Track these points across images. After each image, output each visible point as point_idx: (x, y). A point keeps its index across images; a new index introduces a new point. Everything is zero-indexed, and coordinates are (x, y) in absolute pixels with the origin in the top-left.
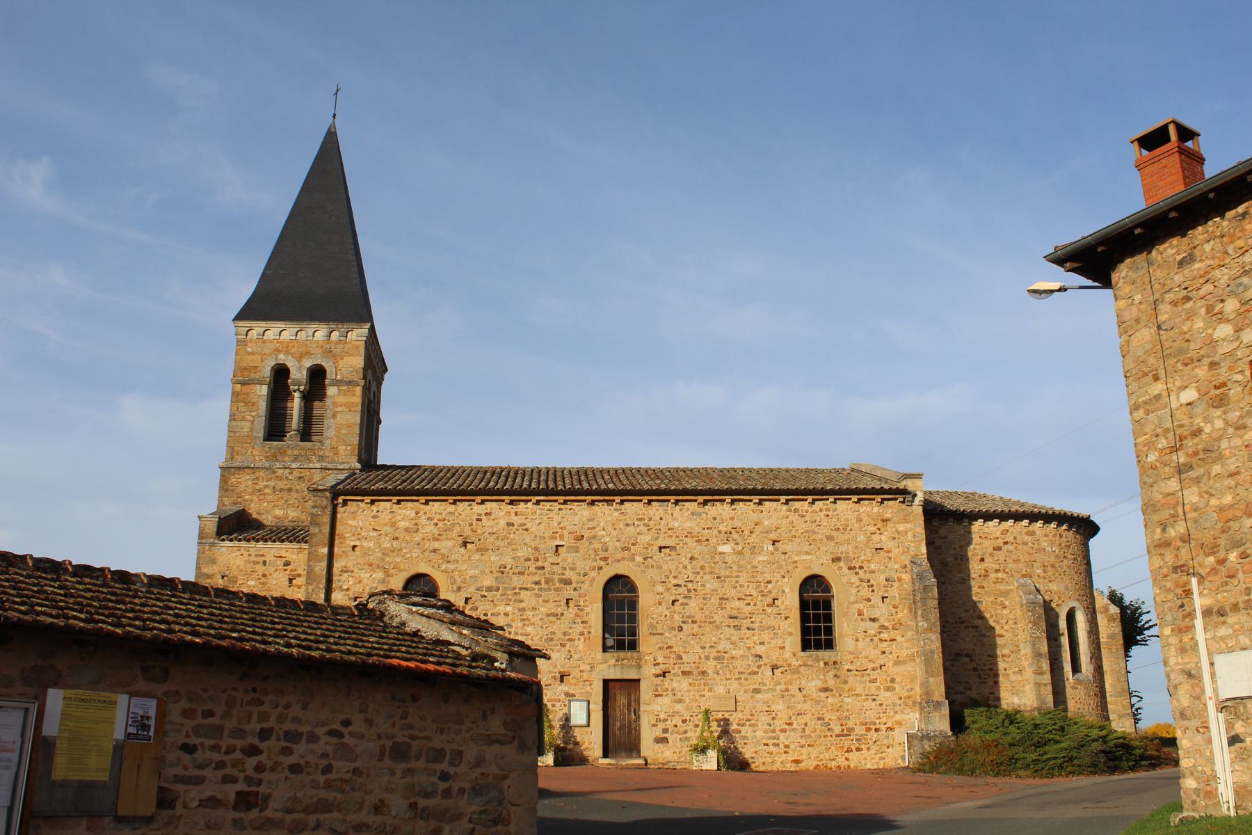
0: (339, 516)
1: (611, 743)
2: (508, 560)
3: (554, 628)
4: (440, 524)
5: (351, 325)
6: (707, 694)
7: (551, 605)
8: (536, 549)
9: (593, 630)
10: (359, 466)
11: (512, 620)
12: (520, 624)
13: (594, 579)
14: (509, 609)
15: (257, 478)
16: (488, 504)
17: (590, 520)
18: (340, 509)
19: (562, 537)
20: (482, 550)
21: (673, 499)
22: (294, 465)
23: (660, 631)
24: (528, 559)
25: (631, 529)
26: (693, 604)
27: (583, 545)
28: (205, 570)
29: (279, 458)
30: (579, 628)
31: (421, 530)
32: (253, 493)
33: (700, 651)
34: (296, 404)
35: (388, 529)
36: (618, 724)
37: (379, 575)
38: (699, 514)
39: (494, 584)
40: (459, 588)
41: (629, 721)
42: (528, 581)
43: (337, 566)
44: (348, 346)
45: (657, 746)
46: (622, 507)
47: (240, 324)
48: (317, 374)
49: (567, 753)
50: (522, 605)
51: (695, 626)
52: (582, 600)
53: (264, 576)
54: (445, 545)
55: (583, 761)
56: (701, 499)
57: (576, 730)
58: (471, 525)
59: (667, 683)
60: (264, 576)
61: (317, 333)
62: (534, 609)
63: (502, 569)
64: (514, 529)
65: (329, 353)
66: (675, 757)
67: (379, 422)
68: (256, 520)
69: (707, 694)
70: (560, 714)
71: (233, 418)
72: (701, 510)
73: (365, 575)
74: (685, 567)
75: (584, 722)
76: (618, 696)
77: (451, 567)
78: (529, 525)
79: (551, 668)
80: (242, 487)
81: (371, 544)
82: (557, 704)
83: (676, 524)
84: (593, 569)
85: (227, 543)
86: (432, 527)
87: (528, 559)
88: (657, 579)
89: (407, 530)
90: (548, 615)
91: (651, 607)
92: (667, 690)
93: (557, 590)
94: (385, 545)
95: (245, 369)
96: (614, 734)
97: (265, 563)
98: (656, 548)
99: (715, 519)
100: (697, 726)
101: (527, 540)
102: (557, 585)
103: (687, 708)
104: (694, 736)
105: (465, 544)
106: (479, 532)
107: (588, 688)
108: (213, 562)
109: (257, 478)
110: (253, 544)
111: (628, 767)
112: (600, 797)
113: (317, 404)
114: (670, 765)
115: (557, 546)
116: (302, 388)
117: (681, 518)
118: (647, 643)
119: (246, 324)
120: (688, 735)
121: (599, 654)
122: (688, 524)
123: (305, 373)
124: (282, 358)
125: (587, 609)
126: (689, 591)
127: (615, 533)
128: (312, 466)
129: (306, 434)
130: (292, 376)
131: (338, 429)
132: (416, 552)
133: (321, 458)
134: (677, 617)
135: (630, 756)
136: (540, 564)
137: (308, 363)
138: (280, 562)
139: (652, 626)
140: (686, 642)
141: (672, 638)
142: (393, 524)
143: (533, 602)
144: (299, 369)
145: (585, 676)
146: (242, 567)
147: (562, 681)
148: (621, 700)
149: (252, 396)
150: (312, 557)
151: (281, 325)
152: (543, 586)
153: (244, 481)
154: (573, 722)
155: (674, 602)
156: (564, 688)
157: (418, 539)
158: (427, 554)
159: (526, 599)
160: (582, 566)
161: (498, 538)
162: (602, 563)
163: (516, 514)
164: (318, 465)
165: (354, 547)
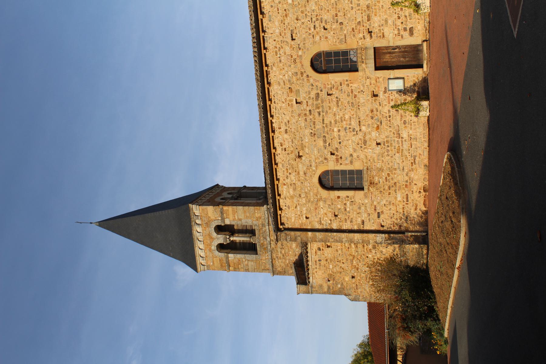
0: (290, 227)
1: (414, 63)
2: (307, 132)
3: (345, 102)
4: (290, 171)
5: (192, 214)
6: (381, 4)
7: (332, 105)
8: (299, 115)
9: (345, 79)
10: (265, 206)
11: (342, 127)
12: (344, 123)
13: (314, 80)
14: (336, 130)
15: (277, 257)
16: (276, 145)
17: (279, 84)
18: (286, 226)
19: (291, 101)
20: (303, 147)
21: (262, 34)
22: (269, 239)
23: (343, 37)
24: (306, 120)
25: (282, 58)
26: (325, 17)
27: (295, 87)
28: (326, 290)
29: (265, 246)
30: (344, 87)
31: (294, 182)
32: (285, 259)
33: (354, 10)
34: (237, 238)
35: (295, 200)
36: (402, 59)
37: (321, 204)
38: (270, 16)
39: (322, 139)
40: (326, 159)
41: (400, 52)
42: (318, 119)
43: (318, 226)
44: (203, 215)
45: (415, 34)
46: (270, 65)
47: (199, 269)
48: (220, 229)
49: (420, 90)
50: (333, 122)
51: (339, 14)
52: (327, 86)
53: (326, 260)
54: (302, 168)
55: (425, 80)
56: (260, 17)
57: (406, 85)
58: (288, 154)
59: (375, 30)
60: (326, 260)
61: (198, 231)
62: (335, 114)
63: (313, 135)
64: (289, 129)
65: (208, 224)
66: (422, 22)
67: (245, 187)
68: (299, 256)
69: (381, 4)
70: (397, 95)
71: (247, 270)
72: (267, 16)
73: (322, 212)
74: (303, 23)
75: (401, 81)
76: (384, 61)
77: (313, 164)
78: (286, 121)
79: (370, 102)
80: (282, 265)
81: (304, 209)
82: (391, 98)
83: (277, 31)
84: (308, 80)
85: (311, 280)
86: (291, 176)
87: (306, 120)
88: (311, 40)
89: (295, 189)
90: (338, 106)
91: (328, 44)
92: (379, 30)
93: (322, 102)
94: (304, 201)
95: (222, 266)
96: (408, 61)
97: (320, 260)
98: (293, 43)
99: (272, 6)
100: (402, 9)
101: (294, 121)
102: (320, 101)
103: (391, 16)
104: (408, 11)
105: (300, 157)
106: (292, 149)
107: (381, 79)
108: (321, 286)
109: (277, 257)
110: (310, 267)
111: (429, 53)
112: (459, 105)
113: (236, 227)
114: (427, 25)
115: (297, 103)
116: (228, 237)
117: (272, 27)
118: (352, 43)
119: (199, 266)
120: (407, 15)
121: (360, 74)
122: (277, 23)
123: (219, 236)
124: (214, 248)
125: (333, 82)
126: (317, 20)
127: (286, 69)
128: (268, 230)
129: (251, 232)
130: (222, 242)
131: (247, 217)
132: (307, 184)
133: (263, 225)
134: (334, 27)
135: (422, 51)
136: (308, 113)
137: (214, 235)
138: (319, 253)
139: (341, 41)
140: (349, 19)
141: (347, 29)
142: (292, 197)
143: (331, 115)
144: (218, 239)
145: (373, 82)
146: (323, 272)
147: (377, 96)
148: (387, 58)
149: (235, 261)
150: (314, 240)
151: (197, 249)
152: (321, 110)
153: (279, 264)
154: (402, 88)
155: (325, 29)
156: (381, 94)
157: (299, 184)
158: (307, 178)
159: (329, 119)
160: (307, 88)
161: (295, 138)
162: (305, 75)
163: (280, 128)
164: (267, 227)
165: (307, 218)
